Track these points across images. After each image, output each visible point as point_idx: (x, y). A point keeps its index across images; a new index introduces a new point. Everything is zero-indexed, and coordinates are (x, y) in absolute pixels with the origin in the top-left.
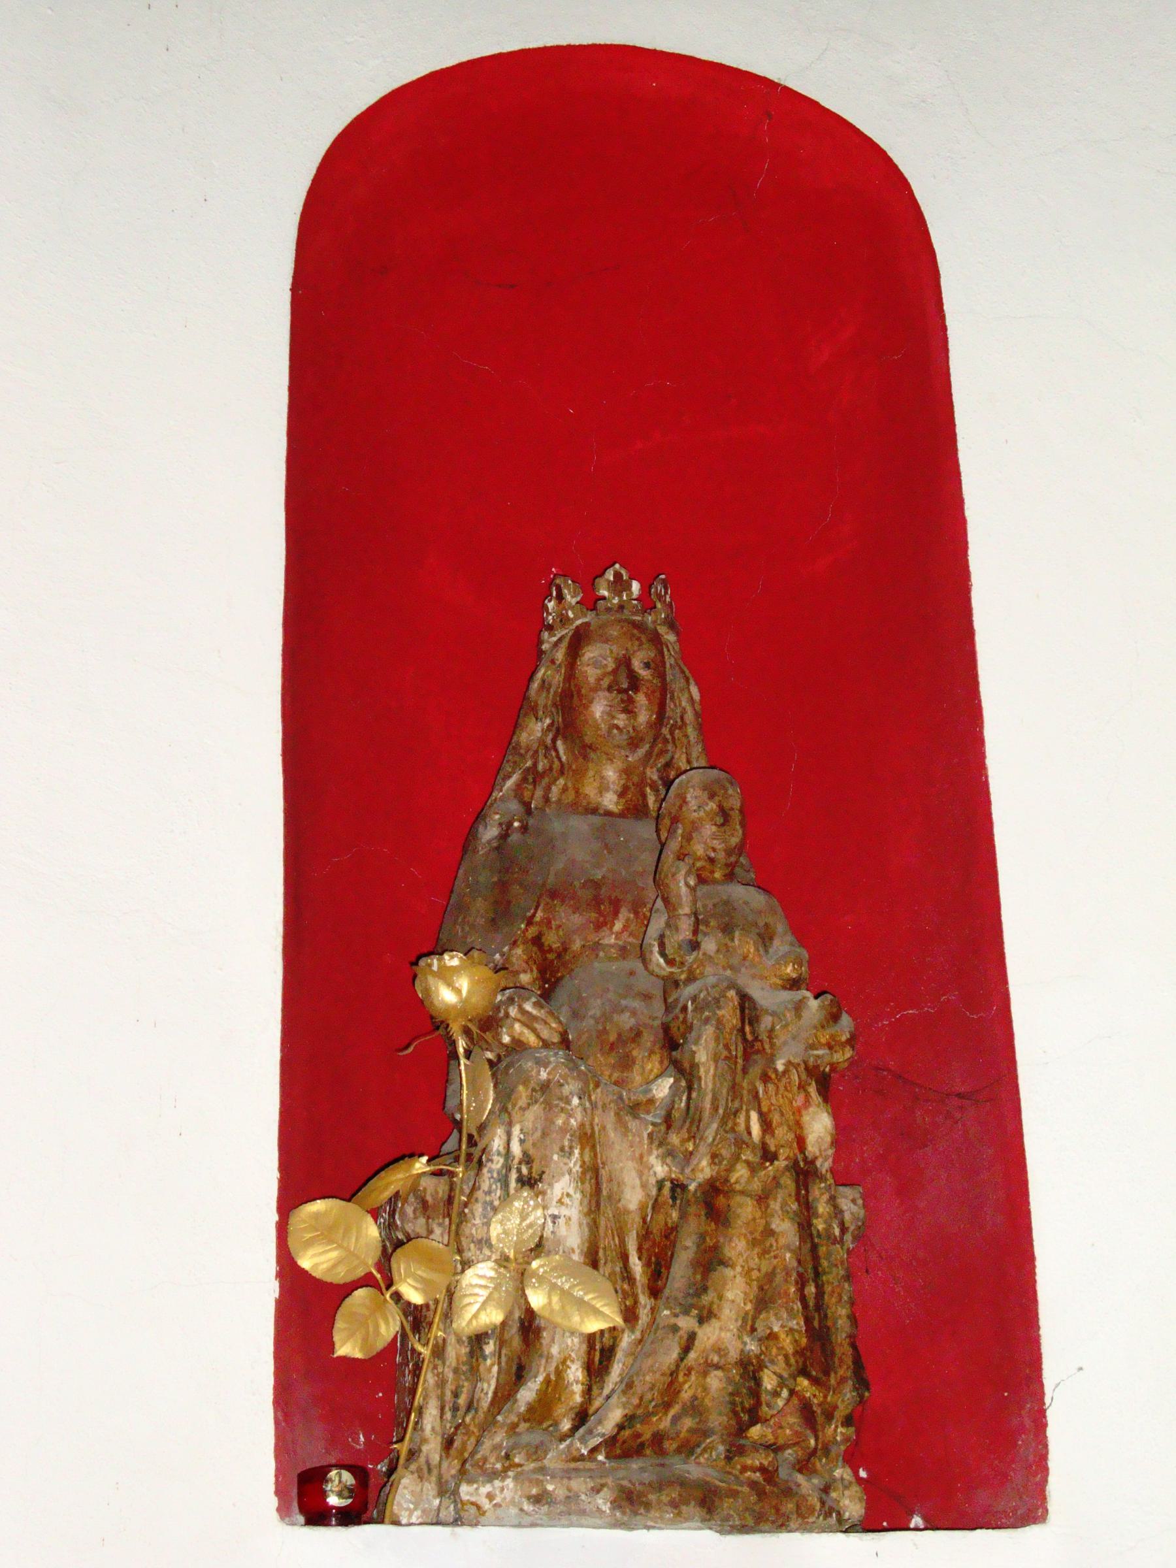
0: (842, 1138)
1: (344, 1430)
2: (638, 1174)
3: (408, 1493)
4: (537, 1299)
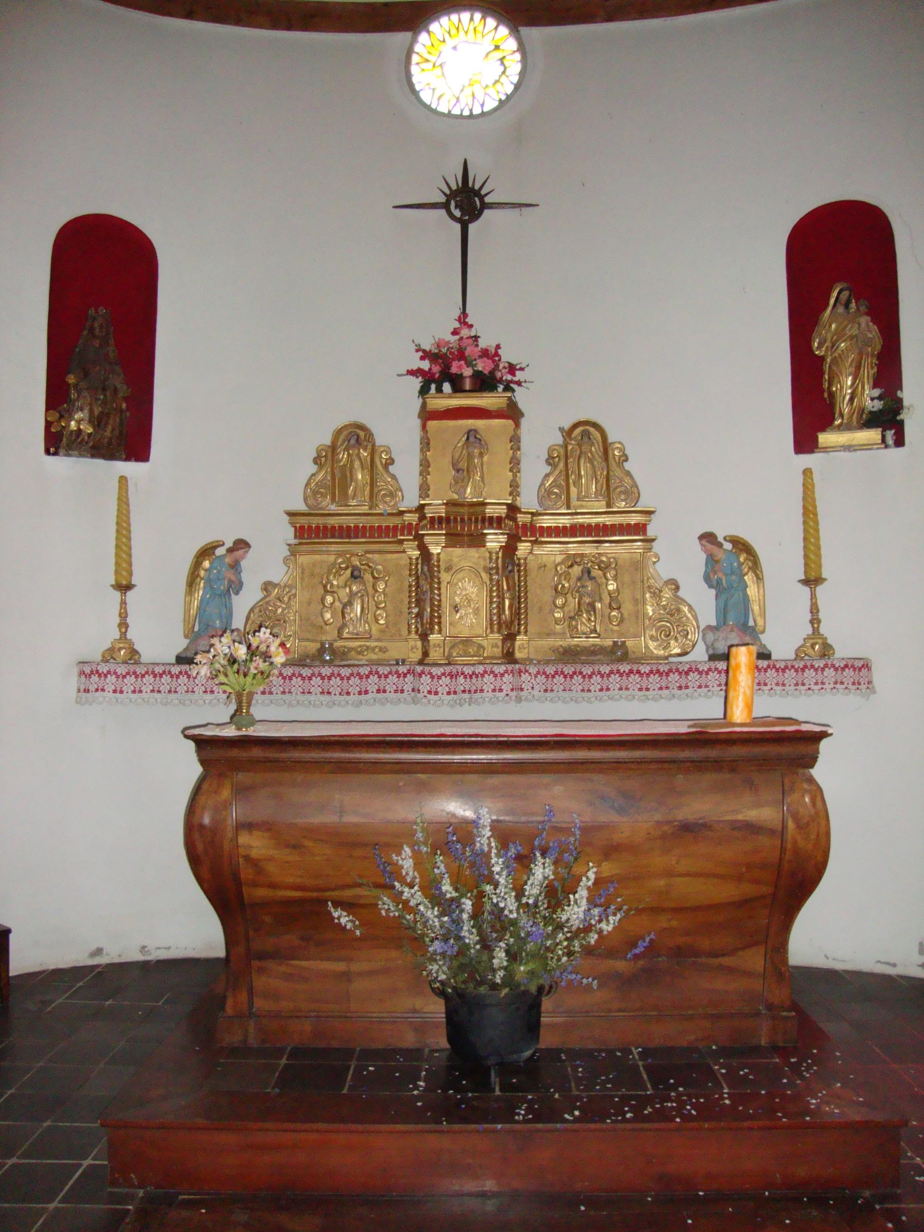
0: (127, 407)
1: (55, 442)
2: (97, 411)
3: (62, 451)
4: (82, 427)
